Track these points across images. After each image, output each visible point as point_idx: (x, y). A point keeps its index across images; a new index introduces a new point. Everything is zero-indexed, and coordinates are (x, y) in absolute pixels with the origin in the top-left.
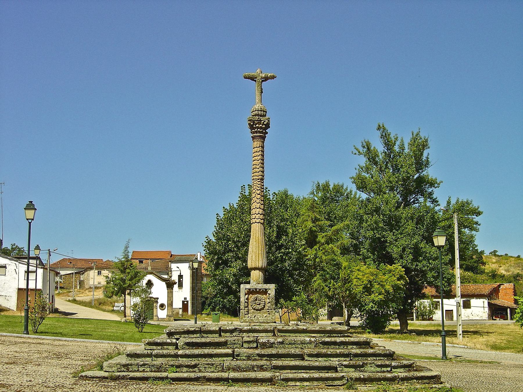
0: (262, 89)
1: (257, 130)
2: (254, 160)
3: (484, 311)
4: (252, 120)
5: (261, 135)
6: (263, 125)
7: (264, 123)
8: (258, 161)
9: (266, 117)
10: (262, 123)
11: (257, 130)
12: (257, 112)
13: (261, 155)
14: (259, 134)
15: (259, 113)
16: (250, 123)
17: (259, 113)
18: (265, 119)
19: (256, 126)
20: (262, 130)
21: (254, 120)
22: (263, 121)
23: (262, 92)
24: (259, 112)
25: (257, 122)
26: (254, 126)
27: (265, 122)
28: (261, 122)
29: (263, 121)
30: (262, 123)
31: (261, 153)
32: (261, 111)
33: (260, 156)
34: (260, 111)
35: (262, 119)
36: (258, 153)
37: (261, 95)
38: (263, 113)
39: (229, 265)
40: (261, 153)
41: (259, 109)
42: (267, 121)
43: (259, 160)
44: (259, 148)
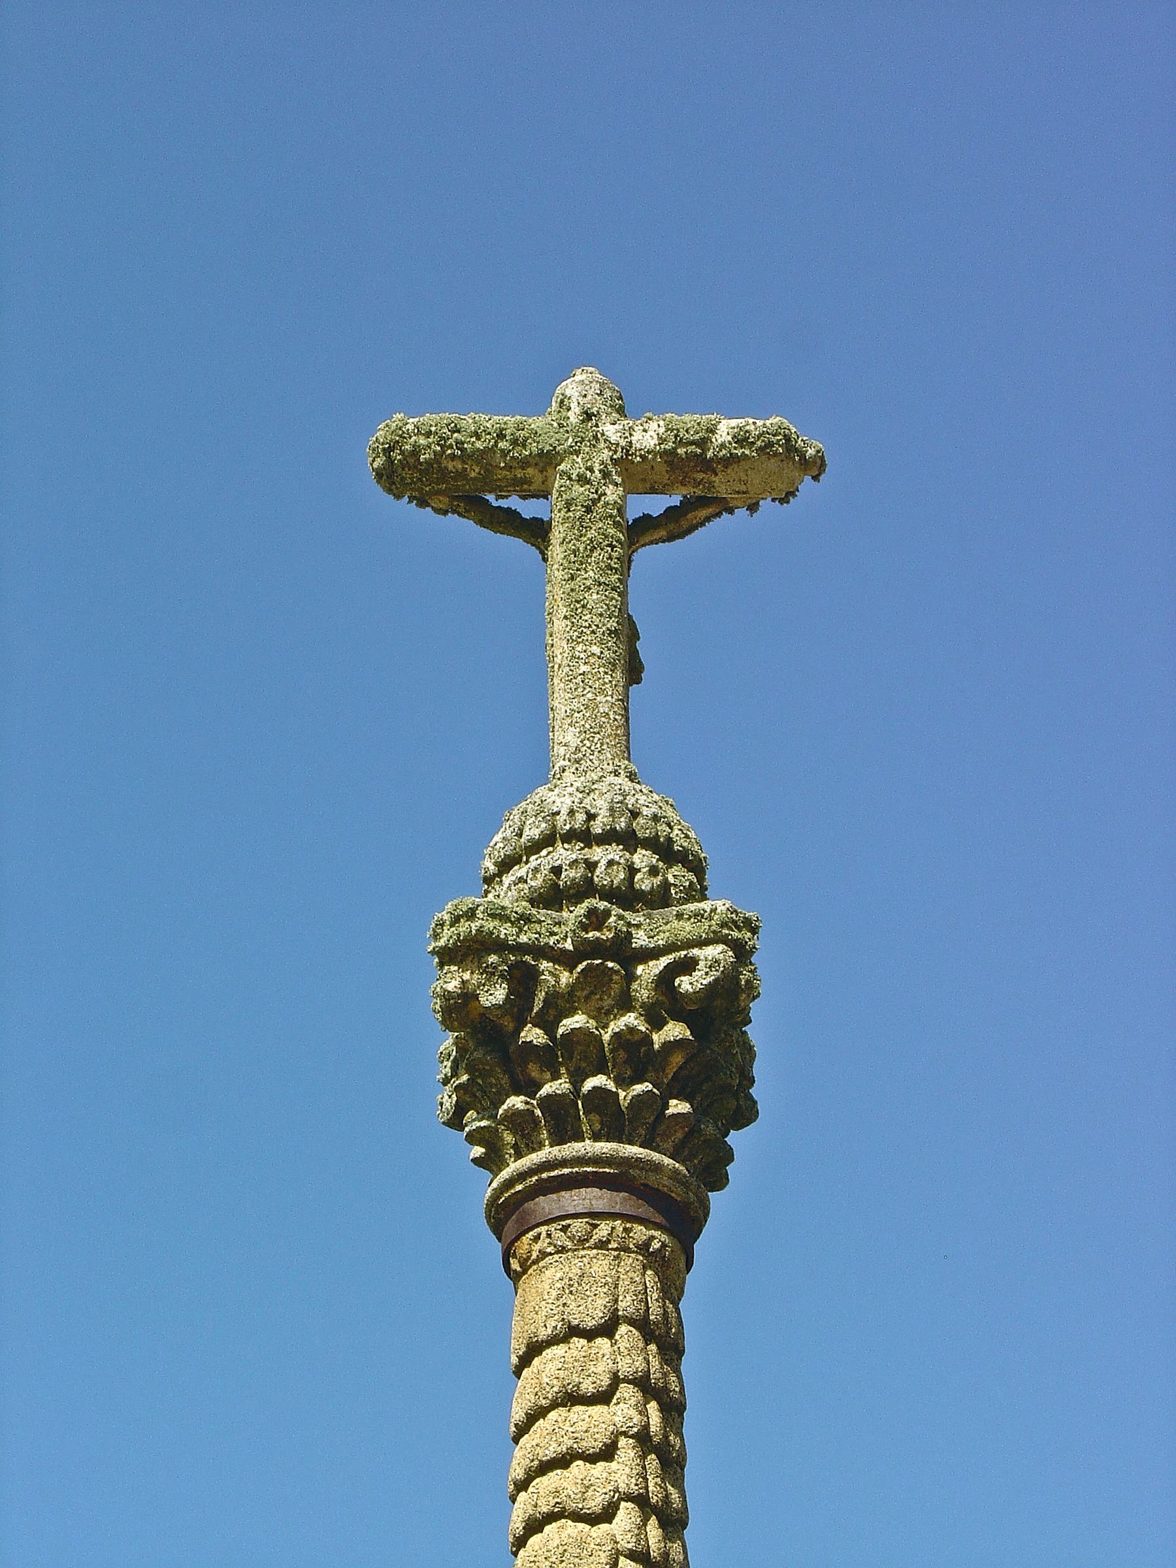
0: (632, 635)
1: (577, 1082)
2: (534, 1526)
3: (659, 422)
4: (501, 946)
5: (628, 1162)
6: (657, 1024)
7: (685, 984)
8: (593, 1520)
9: (706, 906)
10: (642, 991)
11: (577, 1082)
12: (563, 854)
13: (643, 1438)
14: (604, 1147)
15: (591, 866)
16: (467, 996)
17: (591, 866)
18: (687, 929)
19: (550, 1030)
20: (646, 1086)
21: (520, 949)
22: (664, 961)
23: (633, 671)
24: (598, 854)
25: (565, 978)
26: (533, 1035)
27: (688, 965)
28: (631, 977)
29: (664, 961)
30: (642, 991)
31: (644, 1412)
32: (628, 840)
33: (627, 1450)
34: (608, 838)
35: (641, 939)
36: (597, 1410)
37: (554, 1405)
38: (653, 871)
39: (523, 1042)
40: (644, 1412)
41: (591, 817)
42: (713, 951)
43: (607, 1515)
44: (602, 1343)
